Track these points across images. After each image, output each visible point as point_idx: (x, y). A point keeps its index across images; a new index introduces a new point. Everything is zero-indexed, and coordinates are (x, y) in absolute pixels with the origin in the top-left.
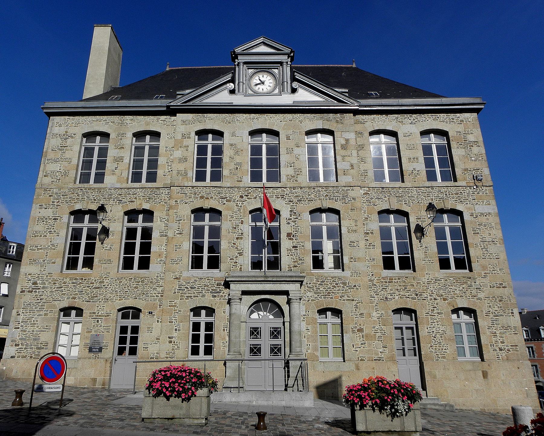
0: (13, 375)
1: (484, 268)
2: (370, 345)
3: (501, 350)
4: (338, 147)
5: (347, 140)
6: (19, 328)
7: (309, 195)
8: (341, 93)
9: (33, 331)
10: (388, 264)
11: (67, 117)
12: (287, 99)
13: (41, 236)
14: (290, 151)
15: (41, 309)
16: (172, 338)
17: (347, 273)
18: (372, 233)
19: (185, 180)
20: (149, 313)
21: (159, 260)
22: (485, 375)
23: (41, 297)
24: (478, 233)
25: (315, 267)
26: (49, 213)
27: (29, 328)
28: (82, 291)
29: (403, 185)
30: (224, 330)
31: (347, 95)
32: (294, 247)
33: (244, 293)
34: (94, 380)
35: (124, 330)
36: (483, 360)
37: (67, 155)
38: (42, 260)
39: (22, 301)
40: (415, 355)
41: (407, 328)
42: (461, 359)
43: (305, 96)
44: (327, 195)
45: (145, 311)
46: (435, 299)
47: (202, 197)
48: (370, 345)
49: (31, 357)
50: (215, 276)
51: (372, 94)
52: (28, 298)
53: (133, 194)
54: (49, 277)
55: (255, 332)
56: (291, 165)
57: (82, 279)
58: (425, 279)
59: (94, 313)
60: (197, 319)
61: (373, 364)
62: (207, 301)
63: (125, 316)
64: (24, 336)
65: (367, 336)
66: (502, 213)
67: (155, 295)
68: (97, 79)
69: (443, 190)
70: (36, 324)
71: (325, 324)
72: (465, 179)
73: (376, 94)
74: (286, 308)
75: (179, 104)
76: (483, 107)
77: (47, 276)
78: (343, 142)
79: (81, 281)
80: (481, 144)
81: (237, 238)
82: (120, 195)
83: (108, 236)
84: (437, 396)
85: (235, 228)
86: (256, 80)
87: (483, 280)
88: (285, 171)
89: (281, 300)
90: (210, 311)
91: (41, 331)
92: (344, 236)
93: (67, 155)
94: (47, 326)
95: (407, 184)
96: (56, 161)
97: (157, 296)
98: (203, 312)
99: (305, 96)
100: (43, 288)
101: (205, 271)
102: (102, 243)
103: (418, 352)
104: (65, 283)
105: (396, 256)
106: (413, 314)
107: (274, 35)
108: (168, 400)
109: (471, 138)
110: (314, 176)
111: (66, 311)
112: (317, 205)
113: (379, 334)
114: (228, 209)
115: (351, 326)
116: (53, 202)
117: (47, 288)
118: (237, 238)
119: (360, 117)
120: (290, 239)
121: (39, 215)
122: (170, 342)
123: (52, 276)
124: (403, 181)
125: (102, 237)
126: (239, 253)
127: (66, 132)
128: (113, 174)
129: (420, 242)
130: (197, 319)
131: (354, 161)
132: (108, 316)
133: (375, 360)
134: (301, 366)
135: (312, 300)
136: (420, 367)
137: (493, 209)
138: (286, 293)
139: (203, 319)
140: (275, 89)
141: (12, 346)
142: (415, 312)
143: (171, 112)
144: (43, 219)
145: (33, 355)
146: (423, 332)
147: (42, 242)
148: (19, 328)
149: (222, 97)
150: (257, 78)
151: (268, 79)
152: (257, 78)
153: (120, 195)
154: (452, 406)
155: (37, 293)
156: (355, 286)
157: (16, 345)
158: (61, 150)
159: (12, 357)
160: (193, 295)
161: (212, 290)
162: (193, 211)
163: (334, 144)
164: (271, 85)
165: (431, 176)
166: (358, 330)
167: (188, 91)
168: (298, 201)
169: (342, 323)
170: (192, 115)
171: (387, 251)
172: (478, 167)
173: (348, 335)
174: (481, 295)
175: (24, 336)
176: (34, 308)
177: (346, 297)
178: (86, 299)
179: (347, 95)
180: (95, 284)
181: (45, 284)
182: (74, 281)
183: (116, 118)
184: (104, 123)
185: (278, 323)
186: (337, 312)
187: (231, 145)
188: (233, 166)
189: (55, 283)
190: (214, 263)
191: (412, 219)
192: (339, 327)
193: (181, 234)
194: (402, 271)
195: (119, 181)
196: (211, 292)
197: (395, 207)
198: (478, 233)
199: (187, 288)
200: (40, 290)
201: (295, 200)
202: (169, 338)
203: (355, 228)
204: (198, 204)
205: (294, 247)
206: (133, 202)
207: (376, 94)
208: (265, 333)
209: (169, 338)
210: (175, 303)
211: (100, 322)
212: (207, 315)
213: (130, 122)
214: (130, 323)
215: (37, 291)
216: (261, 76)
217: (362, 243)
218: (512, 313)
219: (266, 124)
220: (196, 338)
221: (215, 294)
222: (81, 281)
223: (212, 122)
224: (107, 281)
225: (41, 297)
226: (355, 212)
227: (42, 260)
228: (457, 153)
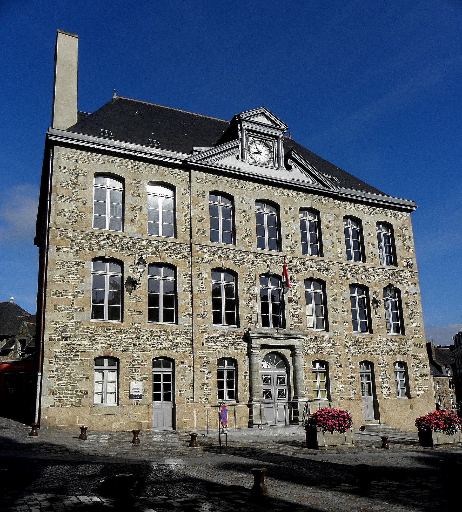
0: (57, 423)
1: (412, 333)
2: (346, 388)
3: (419, 390)
4: (323, 227)
5: (329, 221)
6: (54, 377)
7: (304, 266)
8: (327, 179)
9: (70, 380)
10: (97, 312)
11: (74, 150)
12: (283, 175)
13: (64, 282)
14: (288, 225)
15: (76, 358)
16: (204, 384)
17: (331, 333)
18: (346, 302)
19: (204, 239)
20: (182, 363)
21: (185, 313)
22: (412, 408)
23: (74, 346)
24: (409, 307)
25: (214, 322)
26: (69, 257)
27: (66, 377)
28: (116, 341)
29: (234, 247)
30: (245, 378)
31: (331, 181)
32: (294, 309)
33: (263, 347)
34: (139, 424)
35: (157, 377)
36: (409, 396)
37: (81, 194)
38: (68, 307)
39: (53, 349)
40: (370, 394)
41: (366, 375)
42: (398, 397)
43: (297, 175)
44: (316, 268)
45: (178, 361)
46: (384, 355)
47: (220, 258)
48: (346, 388)
49: (72, 405)
50: (236, 331)
51: (153, 142)
52: (59, 346)
53: (155, 247)
54: (79, 326)
55: (267, 380)
56: (289, 237)
57: (114, 329)
58: (378, 340)
59: (130, 362)
60: (220, 368)
61: (348, 402)
62: (230, 353)
63: (157, 365)
64: (61, 385)
65: (344, 382)
66: (422, 294)
67: (185, 346)
68: (69, 101)
69: (389, 272)
70: (72, 373)
71: (316, 372)
72: (402, 265)
73: (157, 143)
74: (290, 360)
75: (195, 161)
76: (415, 209)
77: (76, 324)
78: (327, 223)
79: (113, 331)
80: (412, 238)
81: (251, 299)
82: (143, 246)
83: (135, 287)
84: (386, 423)
85: (249, 289)
86: (253, 148)
87: (411, 342)
88: (285, 243)
89: (287, 353)
90: (232, 361)
91: (79, 380)
92: (328, 303)
93: (81, 194)
94: (84, 375)
95: (368, 264)
96: (68, 199)
97: (187, 347)
98: (225, 362)
99: (297, 175)
100: (74, 336)
101: (224, 327)
102: (130, 294)
103: (372, 392)
104: (96, 332)
105: (106, 305)
106: (171, 363)
107: (275, 110)
108: (332, 433)
109: (406, 233)
110: (100, 222)
111: (99, 360)
112: (100, 253)
113: (351, 380)
114: (243, 271)
115: (334, 374)
116: (72, 245)
117: (78, 336)
118: (251, 299)
119: (337, 202)
120: (291, 302)
121: (59, 258)
122: (203, 388)
123: (82, 325)
124: (175, 237)
125: (130, 287)
126: (253, 312)
127: (76, 168)
128: (133, 223)
129: (375, 311)
130: (220, 368)
131: (335, 240)
132: (144, 365)
133: (349, 399)
134: (306, 406)
135: (308, 354)
136: (173, 409)
137: (418, 290)
138: (292, 348)
139: (225, 368)
140: (269, 162)
141: (49, 395)
142: (372, 364)
143: (186, 167)
144: (64, 264)
145: (74, 404)
146: (377, 379)
147: (66, 288)
148: (54, 377)
149: (229, 162)
150: (255, 147)
151: (263, 148)
152: (255, 147)
153: (143, 246)
154: (399, 429)
155: (68, 342)
156: (336, 343)
157: (54, 394)
158: (72, 187)
159: (51, 406)
160: (218, 347)
161: (234, 343)
162: (213, 270)
163: (123, 191)
164: (267, 156)
165: (214, 237)
166: (339, 377)
167: (204, 150)
168: (296, 270)
169: (118, 370)
170: (205, 174)
171: (98, 299)
172: (410, 256)
173: (332, 381)
174: (410, 353)
175: (61, 385)
176: (67, 356)
177: (331, 352)
178: (120, 348)
179: (331, 181)
180: (127, 334)
181: (75, 332)
182: (106, 331)
183: (129, 162)
184: (117, 164)
185: (282, 371)
186: (114, 361)
187: (241, 211)
188: (244, 232)
189: (86, 332)
190: (231, 319)
191: (371, 293)
192: (324, 375)
193: (204, 291)
194: (111, 321)
195: (140, 230)
196: (233, 345)
197: (360, 282)
198: (409, 307)
199: (213, 341)
200: (71, 339)
201: (294, 269)
202: (202, 384)
203: (335, 297)
204: (218, 264)
205: (294, 309)
206: (156, 255)
207: (109, 133)
208: (274, 380)
209: (202, 384)
210: (204, 354)
211: (137, 371)
212: (228, 365)
213: (144, 169)
214: (162, 371)
215: (68, 339)
216: (258, 145)
217: (341, 310)
218: (426, 365)
219: (269, 195)
220: (220, 385)
221: (236, 346)
222: (113, 331)
223: (225, 184)
224: (139, 331)
225: (74, 346)
226: (335, 284)
227: (68, 307)
228: (398, 243)
